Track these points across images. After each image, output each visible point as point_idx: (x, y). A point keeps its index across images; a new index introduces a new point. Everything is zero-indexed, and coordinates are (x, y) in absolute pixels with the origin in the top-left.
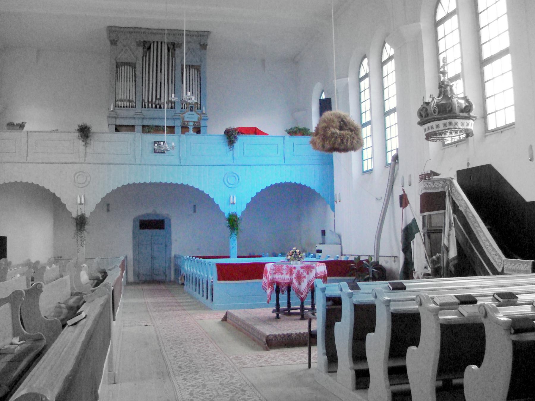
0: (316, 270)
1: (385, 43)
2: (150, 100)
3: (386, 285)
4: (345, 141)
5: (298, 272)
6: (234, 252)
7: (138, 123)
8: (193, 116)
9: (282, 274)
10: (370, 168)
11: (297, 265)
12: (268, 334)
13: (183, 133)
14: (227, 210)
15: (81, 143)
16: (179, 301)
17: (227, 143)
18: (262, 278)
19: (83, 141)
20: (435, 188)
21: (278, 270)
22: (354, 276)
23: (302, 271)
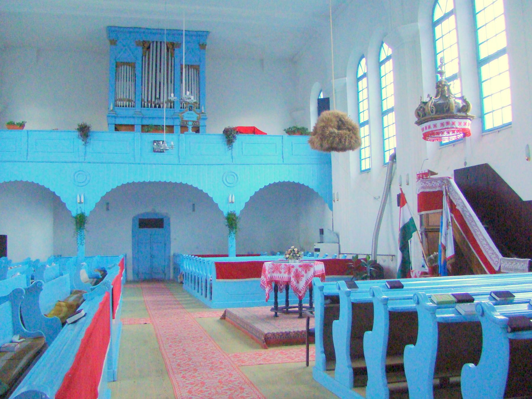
2: (150, 99)
4: (343, 140)
5: (297, 270)
6: (232, 250)
7: (137, 122)
9: (280, 272)
10: (368, 167)
11: (296, 263)
12: (266, 332)
13: (182, 132)
14: (225, 209)
15: (80, 142)
16: (178, 299)
17: (226, 143)
19: (83, 140)
20: (432, 187)
21: (276, 268)
23: (300, 269)
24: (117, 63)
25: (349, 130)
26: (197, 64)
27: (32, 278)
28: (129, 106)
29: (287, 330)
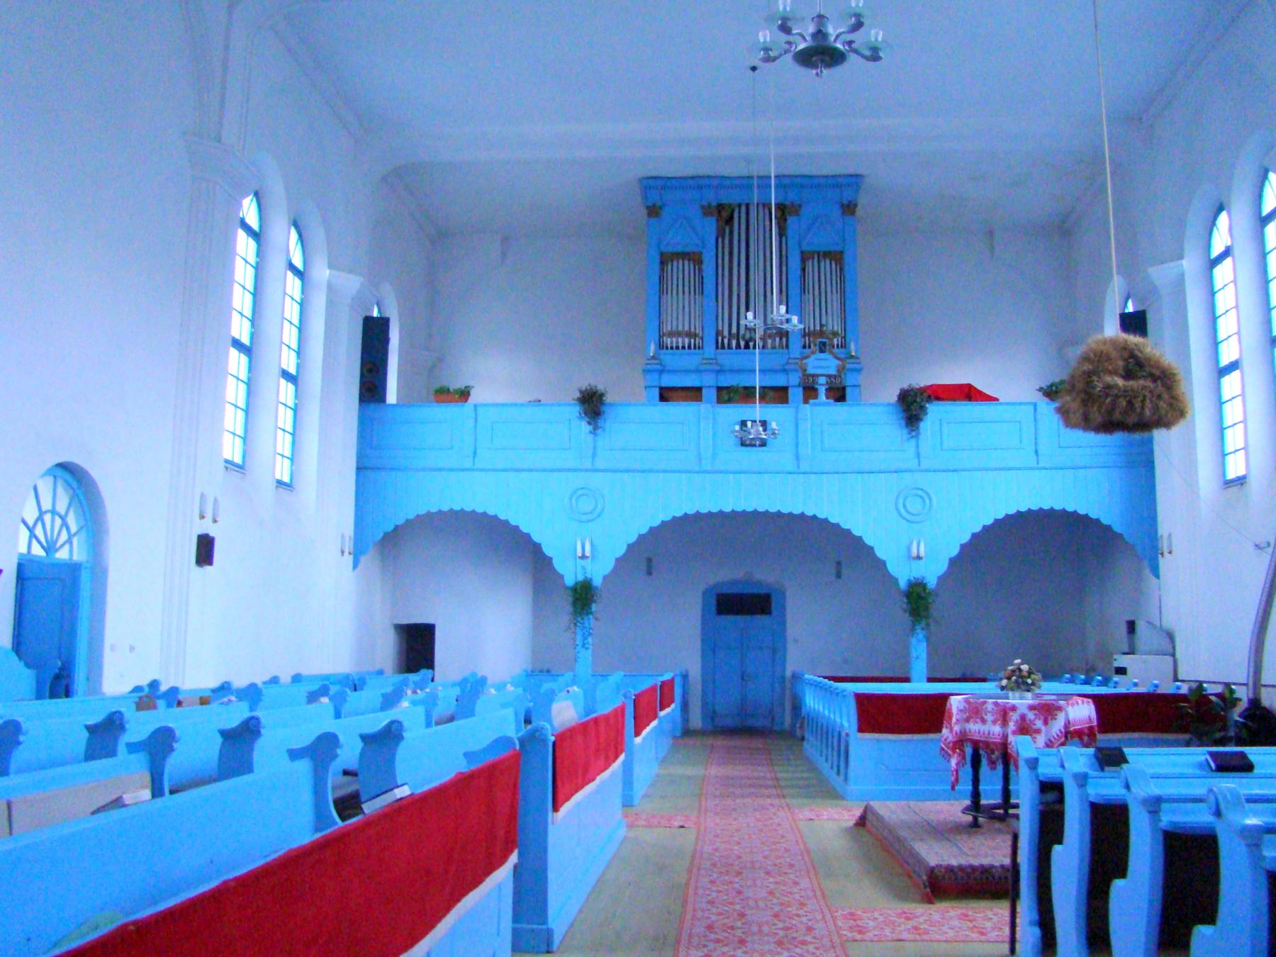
0: (1067, 715)
1: (1266, 172)
2: (734, 330)
3: (1202, 758)
4: (1138, 405)
5: (1023, 717)
6: (919, 667)
7: (708, 381)
8: (823, 363)
9: (984, 721)
10: (1241, 472)
11: (1021, 701)
12: (933, 861)
13: (806, 401)
14: (903, 573)
15: (585, 427)
16: (779, 775)
17: (903, 422)
18: (939, 730)
19: (589, 423)
21: (974, 711)
22: (1186, 731)
23: (1030, 715)
24: (662, 254)
25: (1155, 379)
26: (839, 248)
27: (528, 721)
28: (689, 347)
29: (986, 861)
